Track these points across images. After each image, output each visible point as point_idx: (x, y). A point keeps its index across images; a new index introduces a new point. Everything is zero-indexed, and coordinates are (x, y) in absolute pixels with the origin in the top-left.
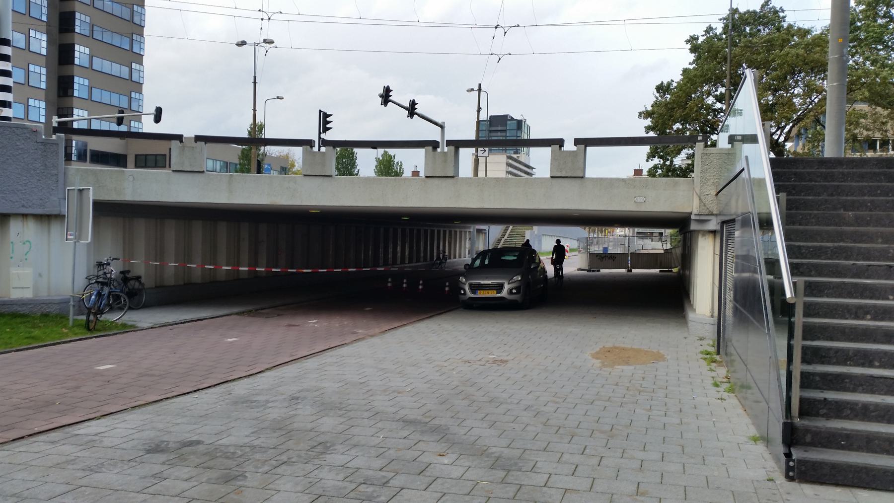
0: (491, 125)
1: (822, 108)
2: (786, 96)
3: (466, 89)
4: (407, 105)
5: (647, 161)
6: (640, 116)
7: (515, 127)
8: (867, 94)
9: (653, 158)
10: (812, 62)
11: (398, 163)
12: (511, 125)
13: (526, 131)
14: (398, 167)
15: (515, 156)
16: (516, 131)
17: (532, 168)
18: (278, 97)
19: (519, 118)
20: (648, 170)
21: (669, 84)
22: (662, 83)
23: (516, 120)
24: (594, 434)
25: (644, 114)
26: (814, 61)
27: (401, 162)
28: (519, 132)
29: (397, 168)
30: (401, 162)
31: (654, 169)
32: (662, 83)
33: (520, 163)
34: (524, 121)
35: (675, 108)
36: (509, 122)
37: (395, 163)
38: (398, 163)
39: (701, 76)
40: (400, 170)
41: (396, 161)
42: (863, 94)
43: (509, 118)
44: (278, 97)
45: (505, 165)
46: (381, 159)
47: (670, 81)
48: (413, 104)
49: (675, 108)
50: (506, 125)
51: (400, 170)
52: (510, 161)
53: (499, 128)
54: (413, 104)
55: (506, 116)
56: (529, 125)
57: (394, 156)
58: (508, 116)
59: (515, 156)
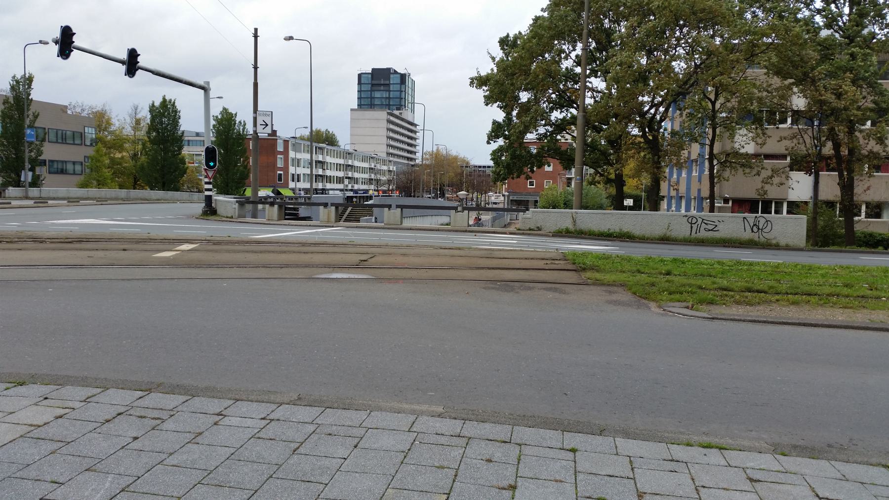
0: (372, 78)
1: (713, 79)
2: (665, 59)
3: (284, 37)
4: (124, 56)
5: (488, 143)
6: (472, 83)
7: (399, 81)
8: (774, 59)
9: (495, 138)
10: (703, 10)
11: (240, 122)
12: (395, 79)
13: (410, 85)
14: (241, 128)
15: (397, 112)
16: (399, 85)
17: (416, 125)
18: (41, 42)
19: (402, 72)
20: (491, 152)
21: (516, 38)
22: (508, 36)
23: (400, 73)
24: (426, 495)
25: (477, 80)
26: (704, 9)
27: (244, 122)
28: (403, 86)
29: (239, 129)
30: (244, 122)
31: (499, 152)
32: (508, 36)
33: (403, 120)
34: (407, 75)
35: (517, 73)
36: (392, 76)
37: (237, 122)
38: (240, 122)
39: (550, 28)
40: (243, 131)
41: (238, 119)
42: (770, 59)
43: (391, 71)
44: (41, 42)
45: (386, 122)
46: (219, 117)
47: (517, 33)
48: (133, 54)
49: (517, 73)
50: (389, 79)
51: (243, 131)
52: (392, 118)
53: (382, 82)
54: (133, 54)
55: (389, 69)
56: (413, 79)
57: (236, 114)
58: (391, 70)
59: (397, 112)
